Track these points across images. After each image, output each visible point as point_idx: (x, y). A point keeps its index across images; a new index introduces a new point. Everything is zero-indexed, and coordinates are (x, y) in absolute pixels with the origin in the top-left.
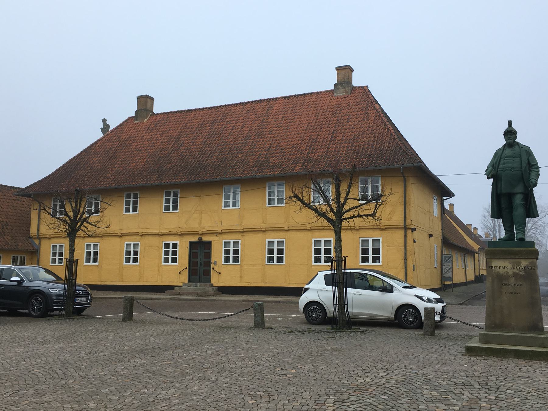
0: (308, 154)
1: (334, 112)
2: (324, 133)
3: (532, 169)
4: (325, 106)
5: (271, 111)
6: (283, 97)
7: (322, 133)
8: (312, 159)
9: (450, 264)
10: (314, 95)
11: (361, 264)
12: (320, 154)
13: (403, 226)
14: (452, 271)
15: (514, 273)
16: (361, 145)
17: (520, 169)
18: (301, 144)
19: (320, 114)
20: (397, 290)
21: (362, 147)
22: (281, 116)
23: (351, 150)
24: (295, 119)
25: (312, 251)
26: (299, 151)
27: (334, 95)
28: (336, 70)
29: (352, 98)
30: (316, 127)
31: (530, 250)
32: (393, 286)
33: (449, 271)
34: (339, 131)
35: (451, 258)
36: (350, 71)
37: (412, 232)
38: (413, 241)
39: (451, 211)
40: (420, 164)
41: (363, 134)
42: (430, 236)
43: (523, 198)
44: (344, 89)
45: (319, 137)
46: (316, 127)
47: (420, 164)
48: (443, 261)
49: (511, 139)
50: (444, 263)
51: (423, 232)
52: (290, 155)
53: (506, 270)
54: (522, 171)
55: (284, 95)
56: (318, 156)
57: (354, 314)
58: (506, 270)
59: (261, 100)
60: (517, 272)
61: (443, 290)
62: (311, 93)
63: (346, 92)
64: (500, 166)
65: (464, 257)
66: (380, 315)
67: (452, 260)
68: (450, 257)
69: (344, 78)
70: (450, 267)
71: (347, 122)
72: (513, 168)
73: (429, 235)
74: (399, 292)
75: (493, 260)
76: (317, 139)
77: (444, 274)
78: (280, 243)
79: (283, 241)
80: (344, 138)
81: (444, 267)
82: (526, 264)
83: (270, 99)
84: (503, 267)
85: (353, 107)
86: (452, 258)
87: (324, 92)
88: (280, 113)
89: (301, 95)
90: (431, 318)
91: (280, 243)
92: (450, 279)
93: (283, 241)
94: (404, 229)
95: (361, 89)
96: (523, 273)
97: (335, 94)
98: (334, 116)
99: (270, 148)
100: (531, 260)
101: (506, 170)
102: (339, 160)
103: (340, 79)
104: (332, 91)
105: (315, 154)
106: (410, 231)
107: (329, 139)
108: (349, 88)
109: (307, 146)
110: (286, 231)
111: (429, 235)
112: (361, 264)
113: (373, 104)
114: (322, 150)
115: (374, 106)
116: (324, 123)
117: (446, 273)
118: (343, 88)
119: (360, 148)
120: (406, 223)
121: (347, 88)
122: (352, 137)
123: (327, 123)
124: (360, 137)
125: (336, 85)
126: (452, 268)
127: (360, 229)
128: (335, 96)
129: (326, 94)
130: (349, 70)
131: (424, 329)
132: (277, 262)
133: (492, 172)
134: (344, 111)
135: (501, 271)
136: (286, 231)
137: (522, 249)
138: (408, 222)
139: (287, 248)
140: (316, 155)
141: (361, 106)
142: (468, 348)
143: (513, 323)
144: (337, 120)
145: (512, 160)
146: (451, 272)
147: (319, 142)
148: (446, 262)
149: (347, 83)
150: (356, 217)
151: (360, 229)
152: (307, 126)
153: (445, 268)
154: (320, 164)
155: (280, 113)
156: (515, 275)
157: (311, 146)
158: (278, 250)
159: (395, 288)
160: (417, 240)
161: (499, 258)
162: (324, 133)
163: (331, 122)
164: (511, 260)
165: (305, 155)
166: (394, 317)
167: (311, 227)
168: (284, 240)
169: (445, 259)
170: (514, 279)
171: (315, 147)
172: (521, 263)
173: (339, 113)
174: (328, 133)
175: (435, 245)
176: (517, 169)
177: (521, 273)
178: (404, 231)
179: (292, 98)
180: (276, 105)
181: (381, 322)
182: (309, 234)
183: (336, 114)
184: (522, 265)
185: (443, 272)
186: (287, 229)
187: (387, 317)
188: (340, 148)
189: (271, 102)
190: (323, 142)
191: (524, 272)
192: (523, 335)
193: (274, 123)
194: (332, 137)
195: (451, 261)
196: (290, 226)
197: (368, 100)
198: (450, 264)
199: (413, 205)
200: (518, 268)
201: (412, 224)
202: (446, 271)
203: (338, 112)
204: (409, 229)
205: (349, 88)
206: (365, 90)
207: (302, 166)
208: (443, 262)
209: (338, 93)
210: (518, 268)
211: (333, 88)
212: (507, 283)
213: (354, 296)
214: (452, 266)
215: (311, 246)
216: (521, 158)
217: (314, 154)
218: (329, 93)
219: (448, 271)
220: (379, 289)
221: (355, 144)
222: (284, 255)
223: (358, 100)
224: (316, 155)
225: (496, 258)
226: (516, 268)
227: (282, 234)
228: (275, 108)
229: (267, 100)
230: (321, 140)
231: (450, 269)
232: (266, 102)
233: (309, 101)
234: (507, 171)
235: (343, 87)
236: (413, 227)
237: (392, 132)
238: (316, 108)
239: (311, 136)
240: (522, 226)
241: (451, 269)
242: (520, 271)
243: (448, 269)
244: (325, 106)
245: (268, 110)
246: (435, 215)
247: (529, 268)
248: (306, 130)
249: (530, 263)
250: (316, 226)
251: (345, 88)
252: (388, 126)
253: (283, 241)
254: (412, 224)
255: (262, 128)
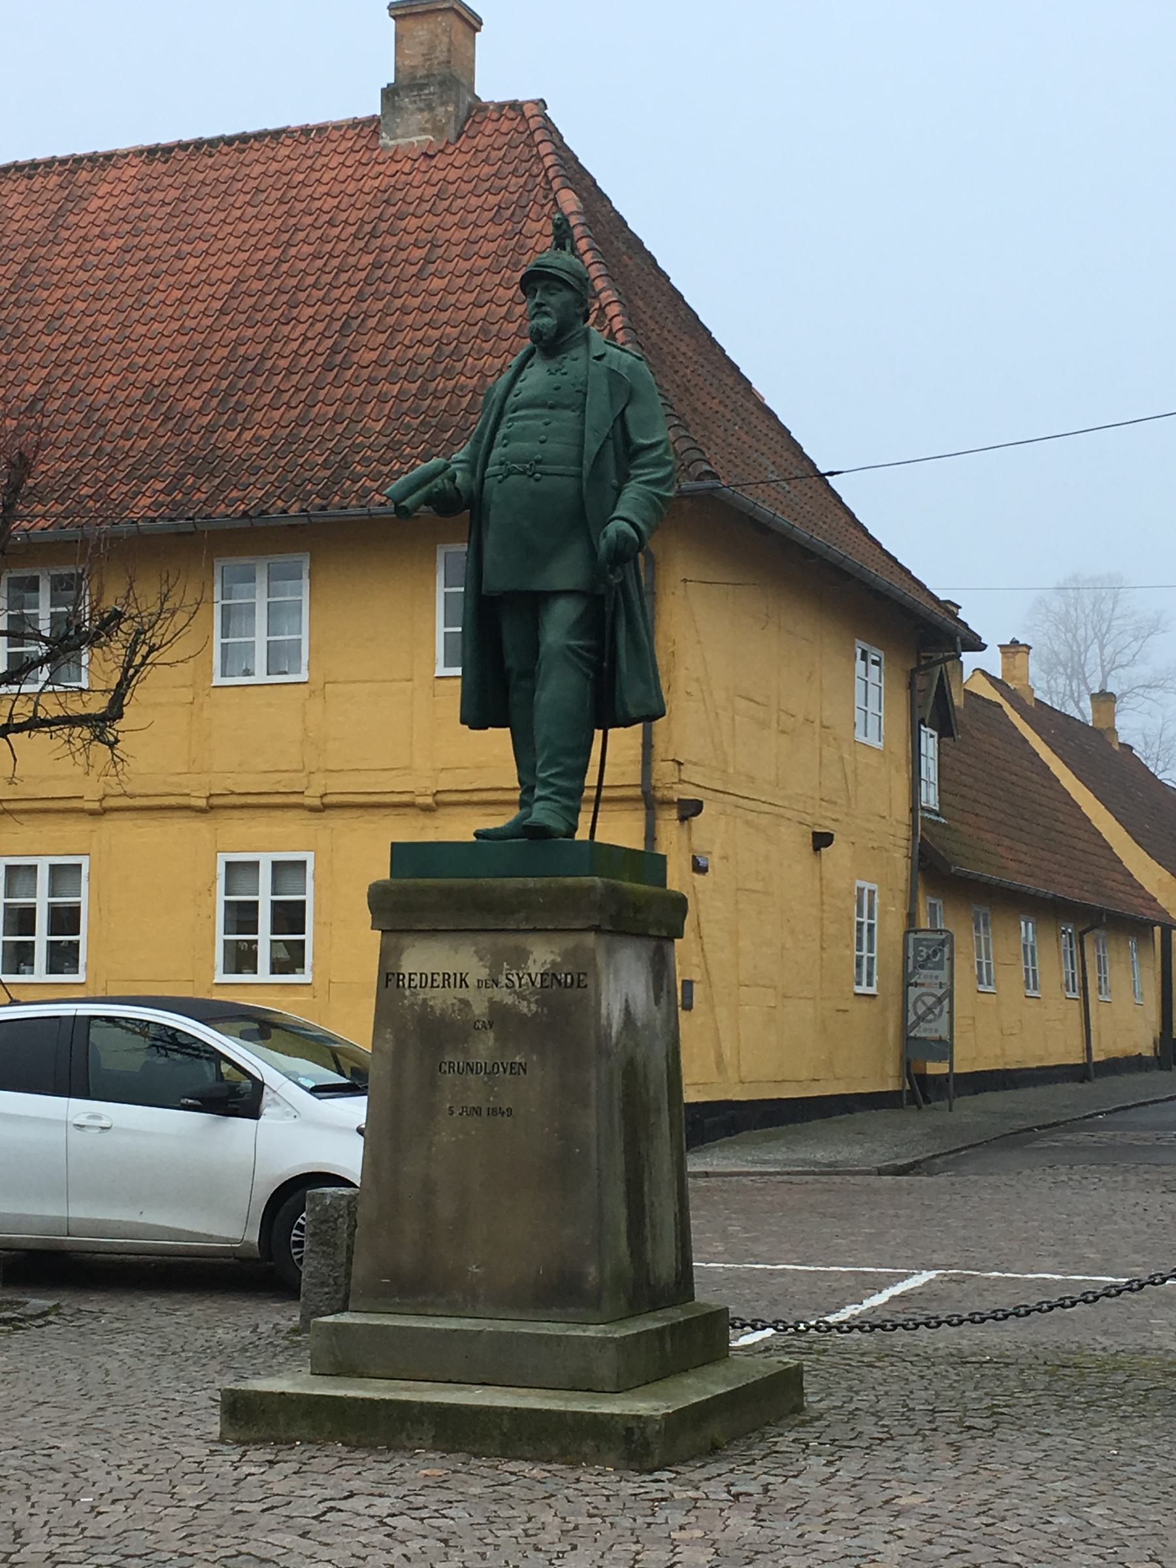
0: (210, 429)
1: (368, 228)
2: (301, 328)
3: (637, 467)
4: (327, 194)
5: (73, 219)
6: (139, 152)
7: (293, 328)
8: (222, 457)
9: (943, 976)
10: (289, 142)
11: (221, 977)
12: (267, 434)
13: (638, 792)
14: (951, 1012)
15: (495, 1007)
16: (462, 388)
17: (573, 469)
18: (185, 380)
19: (301, 235)
20: (277, 1104)
21: (465, 402)
22: (116, 243)
23: (414, 412)
24: (178, 257)
25: (212, 917)
26: (168, 419)
27: (381, 142)
28: (394, 17)
29: (460, 160)
30: (268, 299)
31: (567, 889)
32: (263, 1084)
33: (937, 1011)
34: (372, 322)
35: (946, 950)
36: (458, 25)
37: (683, 818)
38: (688, 865)
39: (1102, 725)
40: (708, 483)
41: (484, 333)
42: (822, 840)
43: (579, 621)
44: (426, 115)
45: (277, 347)
46: (268, 299)
47: (708, 483)
48: (911, 962)
49: (547, 314)
50: (913, 974)
51: (764, 820)
52: (125, 436)
53: (462, 993)
54: (579, 476)
55: (149, 141)
56: (255, 441)
57: (72, 1229)
58: (462, 993)
59: (34, 165)
60: (509, 1000)
61: (913, 1100)
62: (276, 134)
63: (438, 130)
64: (496, 453)
65: (1082, 943)
66: (197, 1234)
67: (951, 959)
68: (942, 943)
69: (427, 57)
70: (940, 992)
71: (419, 276)
72: (538, 462)
73: (815, 834)
74: (287, 1113)
75: (406, 940)
76: (263, 358)
77: (916, 1024)
78: (62, 875)
79: (79, 866)
80: (392, 354)
81: (913, 992)
82: (550, 958)
83: (78, 160)
84: (446, 977)
85: (460, 203)
86: (952, 951)
87: (337, 127)
88: (113, 229)
89: (229, 141)
90: (335, 1246)
91: (62, 875)
92: (943, 1048)
93: (79, 866)
94: (642, 805)
95: (512, 114)
96: (534, 1007)
97: (385, 140)
98: (361, 244)
99: (36, 399)
100: (570, 941)
101: (510, 472)
102: (344, 464)
103: (407, 62)
104: (367, 128)
105: (239, 434)
106: (674, 814)
107: (321, 360)
108: (451, 109)
109: (211, 394)
110: (92, 813)
111: (815, 834)
112: (221, 977)
113: (551, 188)
114: (277, 415)
115: (555, 200)
116: (311, 280)
117: (921, 1019)
118: (421, 110)
119: (459, 403)
120: (655, 776)
121: (440, 110)
122: (430, 351)
123: (326, 278)
124: (466, 349)
125: (389, 94)
126: (950, 994)
127: (439, 804)
128: (385, 148)
129: (343, 136)
130: (452, 17)
131: (302, 1299)
132: (273, 972)
133: (438, 480)
134: (414, 223)
135: (441, 999)
136: (92, 813)
137: (531, 882)
138: (663, 770)
139: (95, 895)
140: (248, 435)
141: (493, 200)
142: (235, 1402)
143: (473, 1268)
144: (376, 266)
145: (540, 423)
146: (945, 1016)
147: (272, 372)
148: (922, 967)
149: (442, 84)
150: (20, 728)
151: (439, 804)
152: (231, 296)
153: (919, 998)
154: (253, 479)
155: (113, 229)
156: (499, 1016)
157: (228, 394)
158: (54, 910)
159: (272, 1095)
160: (725, 858)
161: (435, 931)
162: (301, 328)
163: (344, 277)
164: (485, 940)
165: (196, 438)
166: (256, 1239)
167: (208, 798)
168: (84, 861)
169: (917, 953)
170: (491, 1035)
171: (250, 399)
172: (529, 953)
173: (387, 232)
174: (320, 327)
175: (859, 883)
176: (559, 468)
177: (523, 1007)
178: (641, 815)
179: (181, 155)
180: (105, 189)
181: (183, 1261)
182: (200, 827)
183: (373, 235)
184: (530, 962)
185: (912, 1018)
186: (96, 806)
187: (227, 1240)
188: (363, 402)
189: (84, 176)
190: (289, 372)
191: (537, 1002)
192: (505, 1327)
193: (82, 276)
194: (334, 351)
195: (946, 963)
196: (109, 791)
197: (535, 171)
198: (943, 976)
199: (693, 688)
200: (515, 979)
201: (681, 781)
202: (921, 1009)
203: (384, 226)
204: (667, 803)
205: (451, 109)
206: (527, 121)
207: (166, 491)
208: (910, 969)
209: (399, 131)
210: (515, 979)
211: (372, 107)
212: (458, 1058)
213: (76, 1134)
214: (952, 984)
215: (211, 890)
216: (584, 412)
217: (235, 433)
218: (358, 135)
219: (930, 1010)
220: (184, 1101)
221: (440, 383)
222: (82, 938)
223: (487, 170)
224: (248, 435)
225: (419, 931)
226: (503, 980)
227: (74, 831)
228: (96, 203)
229: (64, 162)
230: (283, 363)
231: (940, 1000)
232: (59, 175)
233: (258, 169)
234: (513, 479)
235: (422, 105)
236: (690, 793)
237: (615, 328)
238: (286, 207)
239: (239, 342)
240: (558, 765)
241: (946, 1002)
242: (522, 997)
243: (930, 1001)
244: (327, 194)
245: (58, 214)
246: (859, 737)
247: (559, 982)
248: (222, 312)
249: (569, 955)
250: (233, 793)
251: (430, 108)
252: (603, 295)
253: (79, 866)
254: (681, 781)
255: (16, 304)
